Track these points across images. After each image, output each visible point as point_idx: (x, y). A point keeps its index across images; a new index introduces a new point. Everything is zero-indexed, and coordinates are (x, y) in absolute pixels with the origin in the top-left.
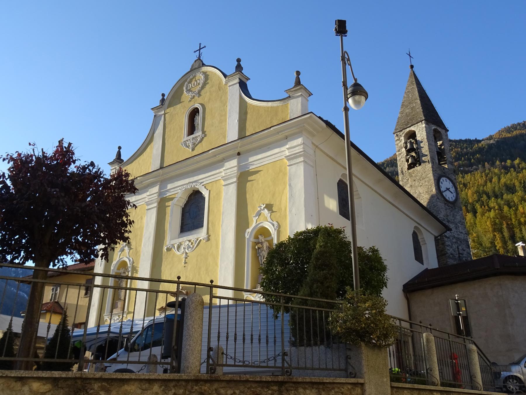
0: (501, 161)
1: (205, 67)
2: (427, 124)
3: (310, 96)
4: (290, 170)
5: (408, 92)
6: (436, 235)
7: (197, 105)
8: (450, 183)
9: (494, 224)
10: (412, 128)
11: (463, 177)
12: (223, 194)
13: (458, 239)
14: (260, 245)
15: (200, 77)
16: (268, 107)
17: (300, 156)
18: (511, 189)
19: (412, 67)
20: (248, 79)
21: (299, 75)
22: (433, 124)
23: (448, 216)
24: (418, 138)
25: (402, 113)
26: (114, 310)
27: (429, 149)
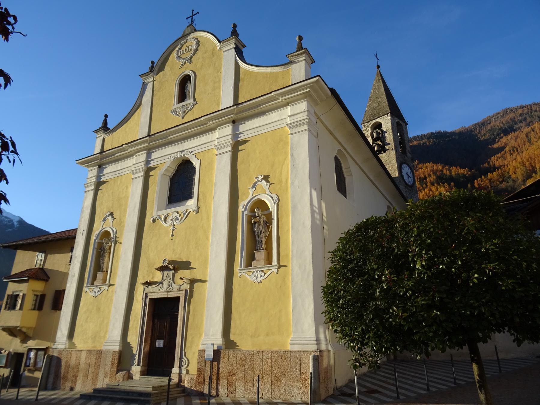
1: (198, 33)
2: (392, 116)
3: (312, 63)
4: (291, 139)
7: (188, 72)
10: (379, 120)
12: (216, 164)
14: (257, 220)
15: (191, 41)
16: (267, 74)
17: (304, 124)
19: (378, 67)
20: (244, 46)
24: (384, 129)
26: (95, 282)
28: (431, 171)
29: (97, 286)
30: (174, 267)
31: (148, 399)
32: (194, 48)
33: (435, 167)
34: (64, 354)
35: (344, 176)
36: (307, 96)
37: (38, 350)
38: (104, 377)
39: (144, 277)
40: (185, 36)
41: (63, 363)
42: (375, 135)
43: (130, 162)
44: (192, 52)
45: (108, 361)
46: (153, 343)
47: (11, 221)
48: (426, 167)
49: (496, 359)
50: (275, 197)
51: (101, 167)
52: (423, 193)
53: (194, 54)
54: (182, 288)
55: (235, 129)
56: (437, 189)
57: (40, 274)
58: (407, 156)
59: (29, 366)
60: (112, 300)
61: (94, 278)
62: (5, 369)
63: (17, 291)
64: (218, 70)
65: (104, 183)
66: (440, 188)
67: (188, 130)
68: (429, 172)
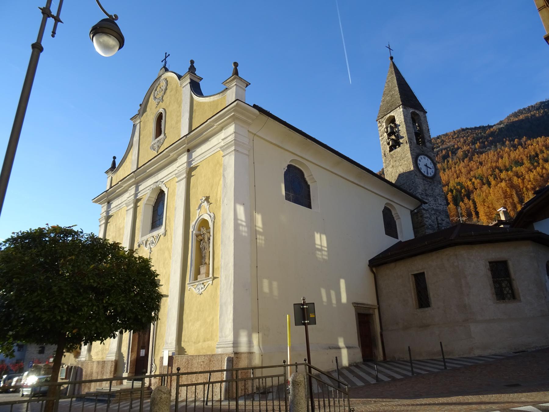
0: (510, 141)
2: (404, 108)
3: (247, 86)
5: (389, 81)
6: (412, 209)
7: (161, 110)
8: (429, 160)
9: (505, 192)
10: (392, 114)
11: (479, 157)
15: (163, 84)
16: (210, 102)
17: (231, 146)
19: (392, 58)
20: (201, 79)
21: (237, 66)
22: (411, 107)
24: (397, 122)
27: (407, 130)
34: (85, 365)
36: (234, 119)
41: (84, 373)
42: (389, 129)
44: (163, 92)
46: (138, 352)
50: (212, 215)
51: (109, 203)
52: (535, 173)
58: (425, 146)
67: (158, 162)
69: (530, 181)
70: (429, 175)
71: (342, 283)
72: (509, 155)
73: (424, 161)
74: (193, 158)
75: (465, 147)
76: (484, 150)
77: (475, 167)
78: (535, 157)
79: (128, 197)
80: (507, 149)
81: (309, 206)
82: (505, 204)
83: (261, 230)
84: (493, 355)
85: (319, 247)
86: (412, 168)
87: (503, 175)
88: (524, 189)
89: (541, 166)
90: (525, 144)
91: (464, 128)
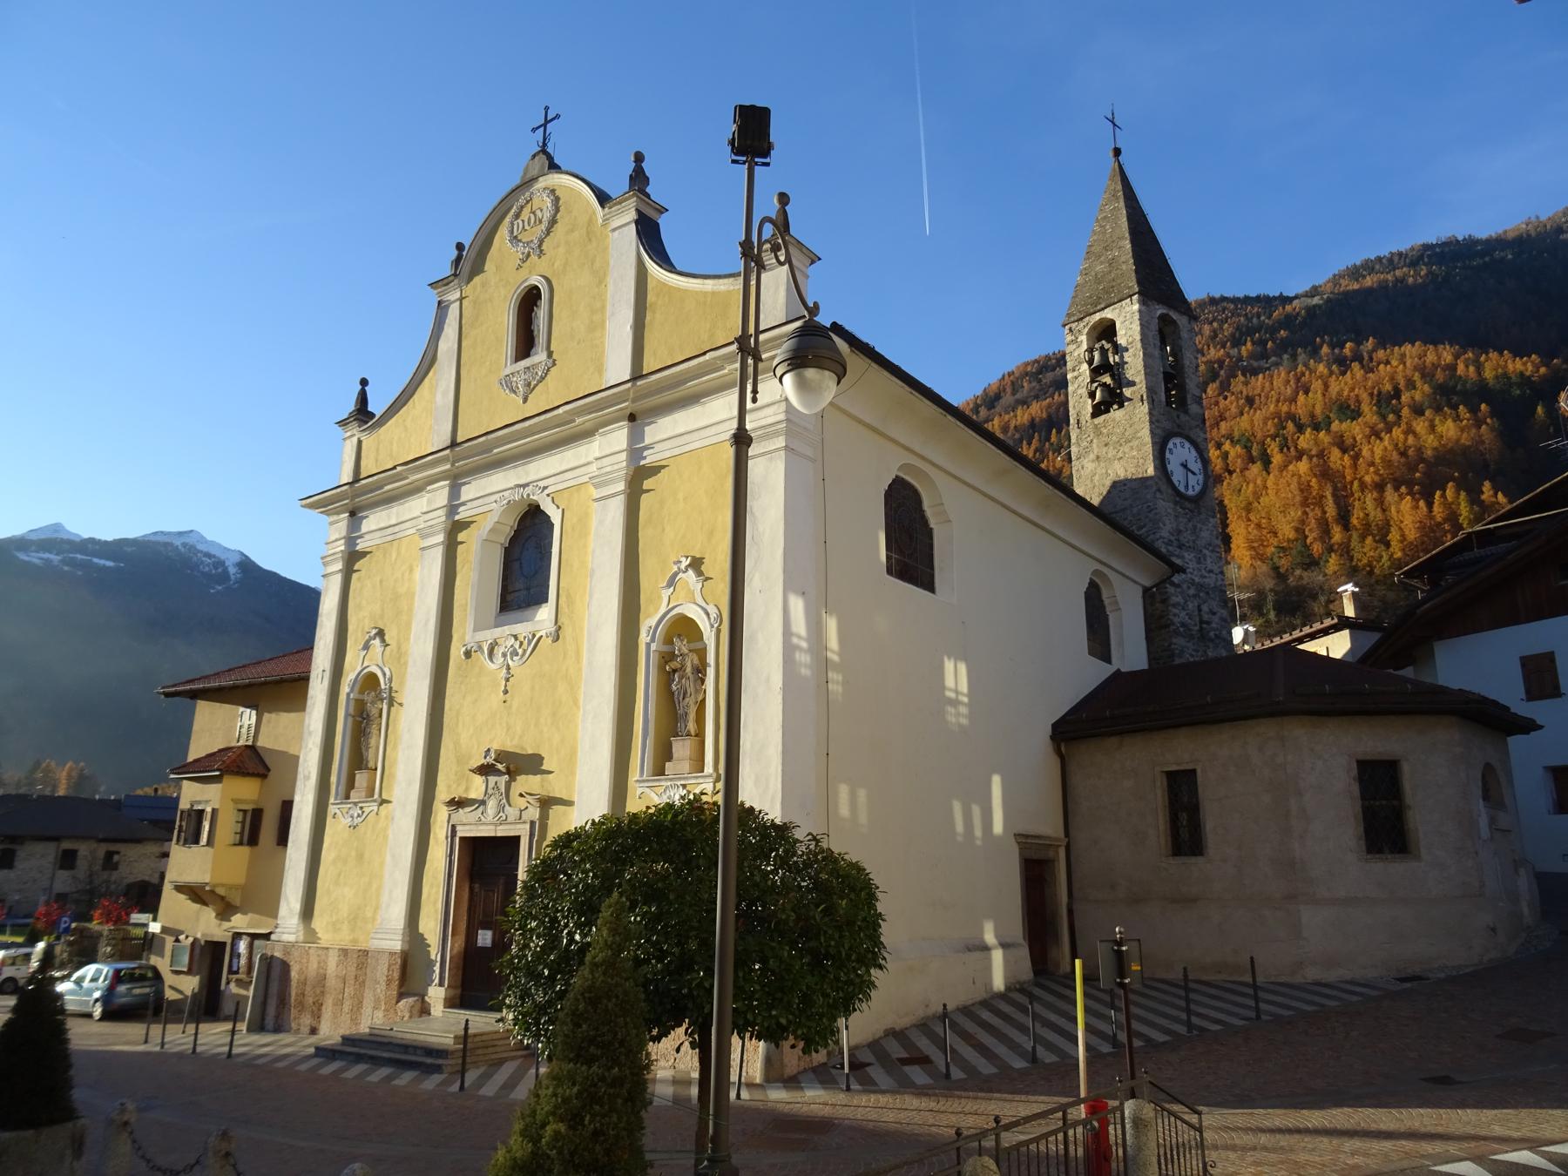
0: (1332, 346)
2: (1142, 302)
3: (813, 262)
6: (1148, 584)
7: (535, 280)
9: (1305, 489)
10: (1108, 314)
11: (1246, 384)
13: (1200, 587)
16: (705, 294)
17: (776, 434)
18: (1349, 411)
19: (1117, 152)
20: (662, 210)
23: (1180, 532)
24: (1121, 340)
25: (1085, 273)
26: (352, 793)
28: (1416, 368)
29: (355, 804)
30: (508, 768)
31: (440, 1061)
32: (547, 215)
33: (1431, 357)
34: (296, 954)
35: (925, 522)
37: (254, 936)
38: (375, 1008)
39: (449, 787)
40: (528, 183)
41: (294, 974)
42: (1097, 355)
43: (415, 506)
44: (543, 227)
45: (382, 975)
47: (220, 563)
48: (1402, 360)
49: (1250, 980)
51: (354, 514)
53: (548, 232)
54: (525, 816)
55: (636, 436)
56: (1432, 428)
57: (248, 762)
58: (1186, 412)
59: (237, 972)
60: (386, 837)
61: (351, 784)
62: (190, 978)
63: (199, 802)
64: (600, 278)
65: (364, 554)
66: (1443, 423)
68: (1408, 372)
69: (1372, 464)
70: (1190, 492)
71: (996, 782)
72: (1326, 386)
73: (1180, 452)
74: (647, 442)
75: (1212, 351)
76: (1263, 363)
77: (1234, 410)
78: (1393, 397)
79: (428, 506)
80: (1321, 368)
81: (930, 587)
82: (1303, 522)
83: (835, 658)
84: (1346, 982)
85: (951, 695)
86: (1151, 471)
87: (1305, 441)
88: (1356, 484)
89: (1403, 426)
90: (1371, 359)
91: (1217, 295)
